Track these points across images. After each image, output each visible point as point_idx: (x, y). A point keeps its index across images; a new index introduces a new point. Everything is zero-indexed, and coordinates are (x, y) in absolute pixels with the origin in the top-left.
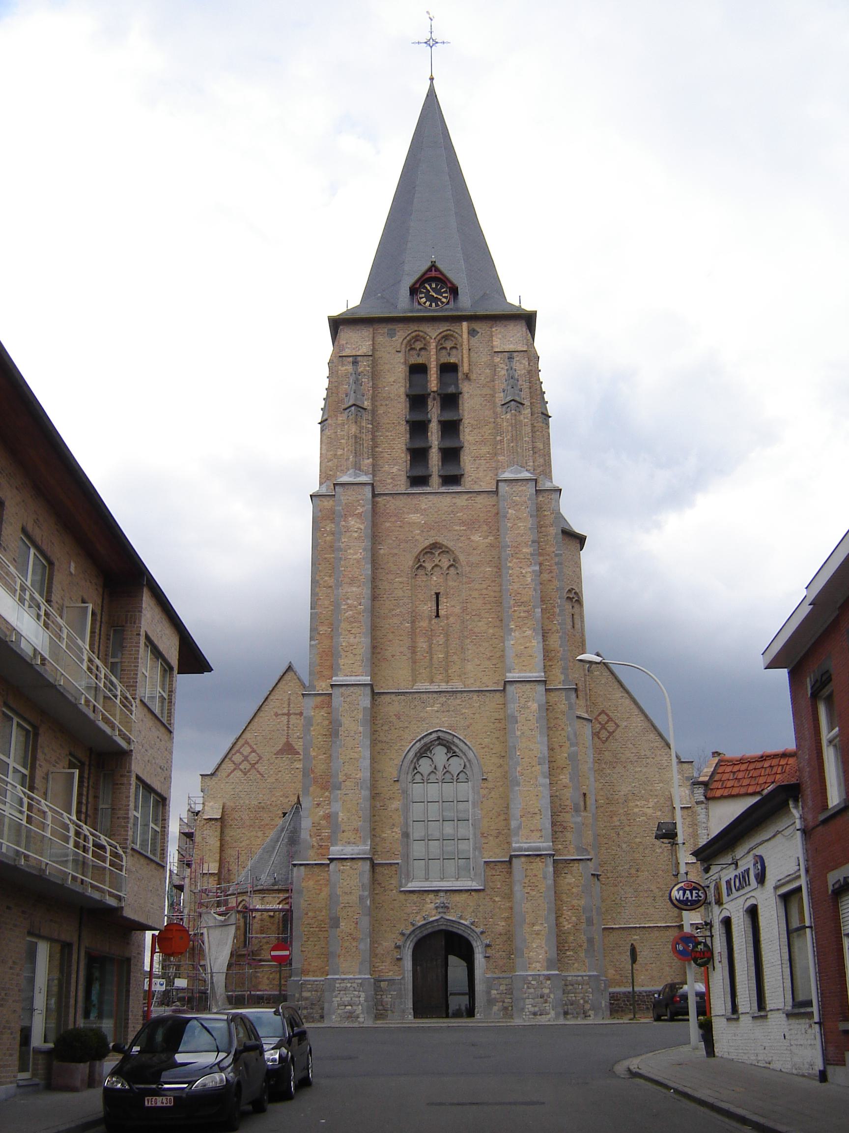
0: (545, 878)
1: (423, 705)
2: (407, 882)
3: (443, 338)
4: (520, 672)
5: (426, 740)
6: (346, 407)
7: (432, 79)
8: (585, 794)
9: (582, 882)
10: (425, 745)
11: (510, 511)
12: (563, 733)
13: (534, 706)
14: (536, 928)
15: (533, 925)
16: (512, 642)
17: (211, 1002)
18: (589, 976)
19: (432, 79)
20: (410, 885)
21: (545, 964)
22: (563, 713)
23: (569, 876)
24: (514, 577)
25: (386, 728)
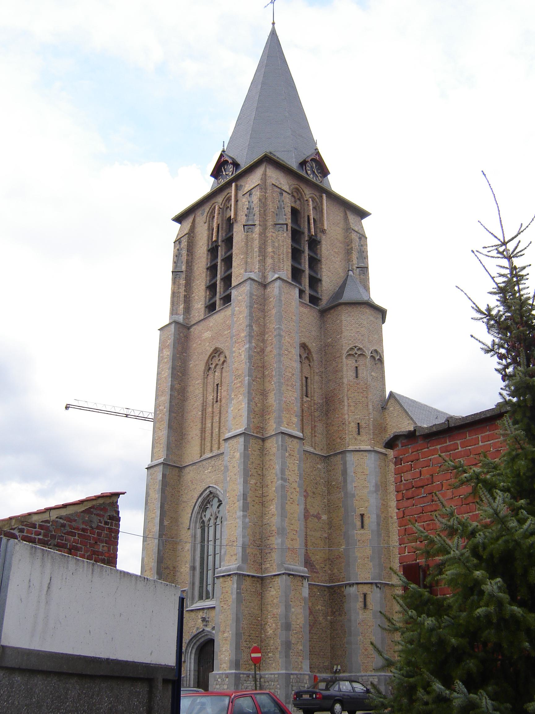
0: (232, 593)
1: (203, 469)
2: (192, 603)
3: (226, 201)
4: (235, 430)
5: (205, 495)
6: (182, 274)
7: (273, 24)
8: (362, 516)
9: (280, 593)
10: (204, 499)
11: (236, 309)
12: (274, 471)
13: (237, 455)
14: (226, 635)
15: (224, 632)
16: (232, 409)
17: (386, 680)
18: (278, 674)
19: (273, 24)
20: (194, 605)
21: (229, 665)
22: (274, 455)
23: (272, 589)
24: (236, 358)
25: (186, 491)
